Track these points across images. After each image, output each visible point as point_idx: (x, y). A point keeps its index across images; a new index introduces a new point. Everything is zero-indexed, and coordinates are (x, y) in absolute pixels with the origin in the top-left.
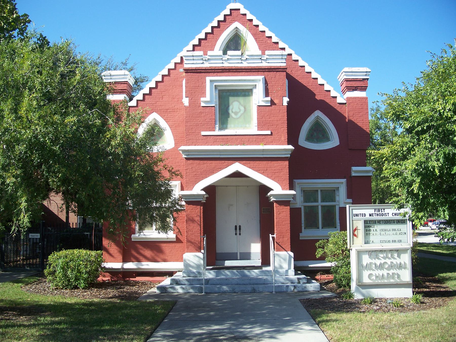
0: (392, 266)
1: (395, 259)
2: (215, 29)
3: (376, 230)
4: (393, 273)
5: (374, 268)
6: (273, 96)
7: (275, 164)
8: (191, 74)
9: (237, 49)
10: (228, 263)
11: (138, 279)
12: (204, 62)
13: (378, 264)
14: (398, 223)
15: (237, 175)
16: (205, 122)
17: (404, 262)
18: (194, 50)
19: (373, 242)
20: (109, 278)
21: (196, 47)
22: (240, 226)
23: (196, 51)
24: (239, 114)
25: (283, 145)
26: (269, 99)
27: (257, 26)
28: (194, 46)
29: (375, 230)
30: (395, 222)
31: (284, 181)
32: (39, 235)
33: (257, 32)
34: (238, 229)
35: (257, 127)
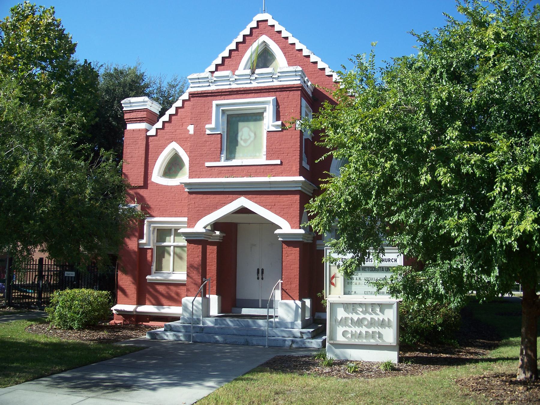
0: (372, 323)
1: (377, 314)
2: (240, 45)
3: (360, 279)
4: (373, 332)
5: (350, 324)
6: (285, 119)
7: (285, 199)
8: (198, 98)
9: (266, 66)
10: (245, 311)
11: (151, 323)
12: (210, 84)
13: (356, 319)
14: (388, 271)
15: (243, 210)
16: (210, 152)
17: (388, 319)
18: (217, 70)
19: (355, 292)
20: (122, 321)
21: (219, 67)
22: (263, 270)
23: (219, 71)
24: (249, 142)
25: (294, 176)
26: (279, 123)
27: (287, 38)
28: (217, 66)
29: (358, 279)
30: (384, 270)
31: (293, 218)
32: (74, 273)
33: (287, 45)
34: (260, 273)
35: (265, 156)
